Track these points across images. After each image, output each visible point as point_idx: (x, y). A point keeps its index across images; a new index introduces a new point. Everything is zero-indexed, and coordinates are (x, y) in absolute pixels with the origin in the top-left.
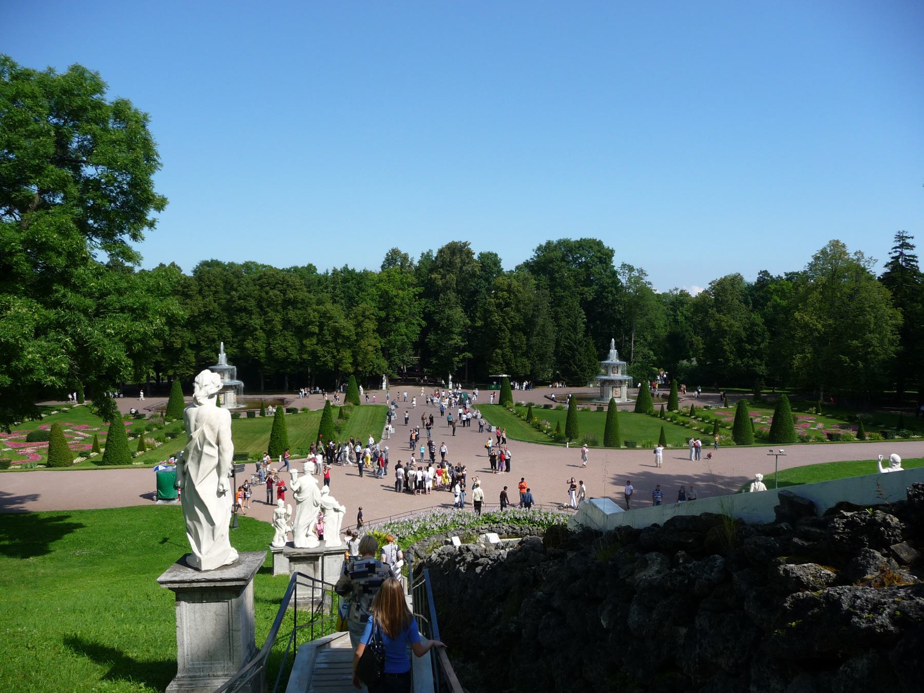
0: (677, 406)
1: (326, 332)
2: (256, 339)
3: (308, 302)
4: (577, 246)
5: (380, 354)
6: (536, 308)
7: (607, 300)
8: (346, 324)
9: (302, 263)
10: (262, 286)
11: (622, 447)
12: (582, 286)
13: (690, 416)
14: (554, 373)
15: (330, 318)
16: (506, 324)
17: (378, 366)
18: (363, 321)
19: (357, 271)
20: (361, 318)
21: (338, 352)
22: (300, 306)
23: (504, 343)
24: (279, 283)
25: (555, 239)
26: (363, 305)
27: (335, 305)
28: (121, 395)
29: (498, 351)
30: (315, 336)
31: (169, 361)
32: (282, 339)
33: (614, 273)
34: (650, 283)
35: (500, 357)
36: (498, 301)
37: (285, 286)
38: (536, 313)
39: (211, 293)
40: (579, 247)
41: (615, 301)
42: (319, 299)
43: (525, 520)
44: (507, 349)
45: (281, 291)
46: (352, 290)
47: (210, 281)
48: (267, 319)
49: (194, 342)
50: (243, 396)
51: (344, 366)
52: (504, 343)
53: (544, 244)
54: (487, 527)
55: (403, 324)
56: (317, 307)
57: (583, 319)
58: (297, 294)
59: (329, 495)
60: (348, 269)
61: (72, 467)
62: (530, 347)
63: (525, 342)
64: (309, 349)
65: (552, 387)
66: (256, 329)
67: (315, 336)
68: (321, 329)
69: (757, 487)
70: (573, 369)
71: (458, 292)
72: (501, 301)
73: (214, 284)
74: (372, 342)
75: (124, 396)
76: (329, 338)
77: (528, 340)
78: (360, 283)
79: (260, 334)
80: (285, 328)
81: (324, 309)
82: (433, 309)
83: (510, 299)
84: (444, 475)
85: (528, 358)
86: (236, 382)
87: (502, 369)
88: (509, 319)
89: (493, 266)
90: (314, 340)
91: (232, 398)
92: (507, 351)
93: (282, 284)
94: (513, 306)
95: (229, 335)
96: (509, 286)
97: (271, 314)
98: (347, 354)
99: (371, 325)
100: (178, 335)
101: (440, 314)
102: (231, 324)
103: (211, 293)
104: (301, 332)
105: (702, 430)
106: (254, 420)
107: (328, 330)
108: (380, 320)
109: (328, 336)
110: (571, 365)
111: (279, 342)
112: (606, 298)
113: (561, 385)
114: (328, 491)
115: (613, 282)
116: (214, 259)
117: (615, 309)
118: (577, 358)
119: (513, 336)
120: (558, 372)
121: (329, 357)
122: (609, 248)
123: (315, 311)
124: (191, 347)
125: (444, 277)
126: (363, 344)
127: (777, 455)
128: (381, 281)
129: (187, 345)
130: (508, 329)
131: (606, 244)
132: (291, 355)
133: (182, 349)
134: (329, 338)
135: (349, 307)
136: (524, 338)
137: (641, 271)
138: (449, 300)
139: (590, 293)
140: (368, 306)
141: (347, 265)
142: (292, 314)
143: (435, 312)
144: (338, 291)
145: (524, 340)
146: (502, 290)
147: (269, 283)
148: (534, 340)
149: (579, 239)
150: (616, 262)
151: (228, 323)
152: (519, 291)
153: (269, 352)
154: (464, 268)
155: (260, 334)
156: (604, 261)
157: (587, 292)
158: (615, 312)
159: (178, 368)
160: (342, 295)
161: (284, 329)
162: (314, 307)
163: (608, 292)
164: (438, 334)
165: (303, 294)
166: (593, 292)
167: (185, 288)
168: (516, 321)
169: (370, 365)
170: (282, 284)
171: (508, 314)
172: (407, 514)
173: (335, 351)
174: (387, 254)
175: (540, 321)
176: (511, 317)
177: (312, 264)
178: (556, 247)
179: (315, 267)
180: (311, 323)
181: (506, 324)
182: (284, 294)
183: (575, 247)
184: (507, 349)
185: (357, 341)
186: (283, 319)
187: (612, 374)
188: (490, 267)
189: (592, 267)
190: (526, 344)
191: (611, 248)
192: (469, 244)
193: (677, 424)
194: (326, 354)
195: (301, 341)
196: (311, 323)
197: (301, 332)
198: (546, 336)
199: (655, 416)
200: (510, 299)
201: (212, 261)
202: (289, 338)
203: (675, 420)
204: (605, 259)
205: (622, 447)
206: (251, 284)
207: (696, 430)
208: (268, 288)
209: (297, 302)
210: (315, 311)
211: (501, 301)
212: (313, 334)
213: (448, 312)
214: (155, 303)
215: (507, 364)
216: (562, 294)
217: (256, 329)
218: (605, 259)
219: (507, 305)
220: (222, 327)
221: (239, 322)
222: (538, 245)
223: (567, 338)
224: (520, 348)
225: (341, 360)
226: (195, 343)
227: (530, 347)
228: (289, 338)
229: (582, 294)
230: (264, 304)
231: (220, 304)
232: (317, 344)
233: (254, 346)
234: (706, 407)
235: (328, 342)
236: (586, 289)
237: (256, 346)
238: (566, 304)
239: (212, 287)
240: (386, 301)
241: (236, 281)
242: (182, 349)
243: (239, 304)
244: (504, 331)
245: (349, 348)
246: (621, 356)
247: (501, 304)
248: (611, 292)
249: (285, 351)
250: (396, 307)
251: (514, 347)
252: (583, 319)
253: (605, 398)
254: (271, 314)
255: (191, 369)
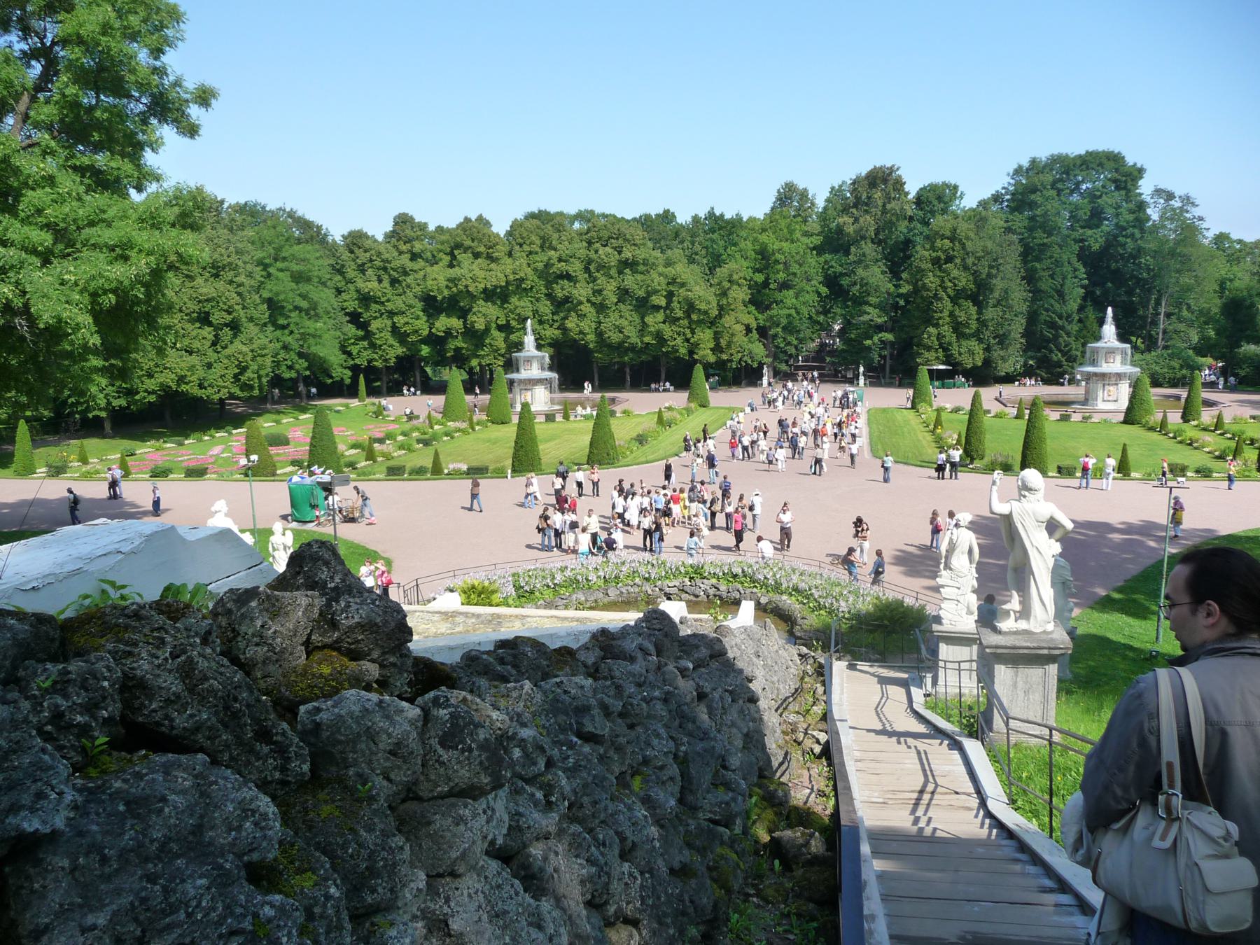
0: (1199, 415)
1: (675, 305)
2: (582, 316)
3: (653, 264)
4: (1079, 162)
5: (755, 335)
6: (995, 265)
7: (1125, 249)
8: (703, 294)
9: (655, 210)
10: (590, 243)
11: (1050, 474)
12: (1082, 227)
13: (1214, 431)
14: (1025, 365)
15: (683, 285)
16: (945, 289)
17: (750, 353)
18: (729, 289)
19: (728, 216)
20: (726, 285)
21: (693, 332)
22: (641, 268)
23: (940, 318)
24: (612, 238)
25: (1043, 154)
26: (732, 265)
27: (692, 266)
28: (418, 392)
29: (931, 329)
30: (662, 311)
31: (472, 347)
32: (617, 314)
33: (1142, 206)
34: (1201, 219)
35: (934, 338)
36: (934, 255)
37: (621, 241)
38: (994, 271)
39: (524, 254)
40: (1081, 165)
41: (1139, 251)
42: (667, 259)
43: (745, 576)
44: (946, 328)
45: (615, 248)
46: (718, 245)
47: (522, 238)
48: (596, 288)
49: (502, 322)
50: (558, 395)
51: (701, 353)
52: (940, 318)
53: (1026, 164)
54: (677, 584)
55: (791, 292)
56: (664, 270)
57: (1081, 279)
58: (637, 252)
59: (226, 515)
60: (714, 214)
61: (276, 478)
62: (983, 323)
63: (975, 317)
64: (652, 329)
65: (1019, 386)
66: (581, 303)
67: (662, 311)
68: (669, 301)
69: (954, 538)
70: (1055, 358)
71: (877, 241)
72: (940, 253)
73: (528, 242)
74: (741, 318)
75: (422, 393)
76: (679, 314)
77: (979, 313)
78: (731, 234)
79: (586, 308)
80: (620, 300)
81: (673, 272)
82: (839, 269)
83: (954, 250)
84: (682, 504)
85: (980, 341)
86: (548, 374)
87: (937, 358)
88: (950, 281)
89: (935, 202)
90: (660, 316)
91: (542, 395)
92: (946, 330)
93: (617, 239)
94: (958, 261)
95: (548, 311)
96: (954, 230)
97: (601, 280)
98: (705, 337)
99: (740, 294)
100: (481, 312)
101: (850, 276)
102: (549, 296)
103: (524, 254)
104: (643, 306)
105: (1217, 453)
106: (551, 425)
107: (679, 302)
108: (753, 285)
109: (677, 311)
110: (1051, 351)
111: (609, 322)
112: (1123, 245)
113: (1033, 382)
114: (225, 509)
115: (1137, 219)
116: (542, 208)
117: (1141, 263)
118: (1061, 340)
119: (956, 307)
120: (1031, 362)
121: (679, 341)
122: (1135, 164)
123: (660, 275)
124: (500, 328)
125: (856, 220)
126: (728, 320)
127: (1171, 488)
128: (764, 230)
129: (494, 325)
130: (949, 297)
131: (1130, 160)
132: (629, 337)
133: (487, 330)
134: (679, 314)
135: (712, 270)
136: (973, 310)
137: (1187, 200)
138: (864, 255)
139: (1095, 237)
140: (739, 267)
141: (713, 209)
142: (630, 280)
143: (842, 275)
144: (698, 247)
145: (974, 313)
146: (943, 237)
147: (600, 238)
148: (990, 313)
149: (1083, 152)
150: (1145, 188)
151: (546, 295)
152: (967, 238)
153: (599, 334)
154: (889, 207)
155: (586, 308)
156: (1123, 185)
157: (1091, 237)
158: (1141, 268)
159: (483, 357)
160: (704, 252)
161: (619, 301)
162: (661, 269)
163: (1126, 236)
164: (848, 307)
165: (646, 252)
166: (1101, 237)
167: (490, 247)
168: (962, 283)
169: (739, 352)
170: (617, 239)
171: (949, 274)
172: (812, 562)
173: (688, 332)
174: (779, 191)
175: (999, 284)
176: (954, 278)
177: (668, 210)
178: (1044, 167)
179: (673, 213)
180: (656, 292)
181: (945, 289)
182: (620, 253)
183: (1074, 166)
184: (946, 328)
185: (720, 316)
186: (619, 288)
187: (1104, 365)
188: (931, 202)
189: (1100, 196)
190: (977, 319)
191: (1139, 165)
192: (898, 169)
193: (1181, 442)
194: (676, 336)
195: (642, 318)
196: (656, 292)
197: (643, 306)
198: (1011, 307)
199: (1152, 429)
200: (954, 250)
201: (540, 211)
202: (627, 314)
203: (1180, 436)
204: (1126, 182)
205: (1050, 474)
206: (577, 238)
207: (1209, 453)
208: (598, 245)
209: (637, 264)
210: (660, 275)
211: (940, 253)
212: (657, 308)
213: (860, 272)
214: (144, 238)
215: (945, 350)
216: (1045, 241)
217: (581, 303)
218: (1126, 182)
219: (949, 259)
220: (538, 300)
221: (559, 294)
222: (1016, 166)
223: (1047, 310)
224: (967, 325)
225: (697, 345)
226: (504, 322)
227: (983, 323)
228: (627, 314)
229: (1082, 241)
230: (592, 267)
231: (535, 270)
232: (664, 322)
233: (578, 326)
234: (1253, 417)
235: (679, 319)
236: (1089, 232)
237: (582, 326)
238: (1051, 257)
239: (525, 246)
240: (765, 259)
241: (556, 236)
242: (487, 330)
243: (558, 269)
244: (941, 299)
245: (710, 328)
246: (1122, 337)
247: (939, 258)
248: (1133, 234)
249: (621, 332)
250: (781, 267)
251: (957, 327)
252: (1081, 279)
253: (1091, 402)
254: (601, 280)
255: (500, 358)
